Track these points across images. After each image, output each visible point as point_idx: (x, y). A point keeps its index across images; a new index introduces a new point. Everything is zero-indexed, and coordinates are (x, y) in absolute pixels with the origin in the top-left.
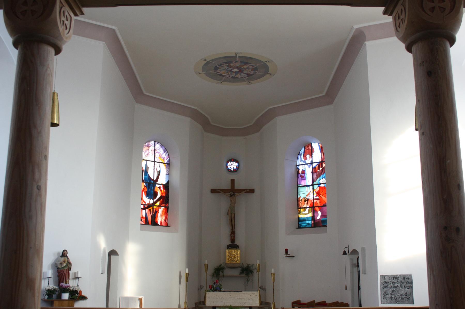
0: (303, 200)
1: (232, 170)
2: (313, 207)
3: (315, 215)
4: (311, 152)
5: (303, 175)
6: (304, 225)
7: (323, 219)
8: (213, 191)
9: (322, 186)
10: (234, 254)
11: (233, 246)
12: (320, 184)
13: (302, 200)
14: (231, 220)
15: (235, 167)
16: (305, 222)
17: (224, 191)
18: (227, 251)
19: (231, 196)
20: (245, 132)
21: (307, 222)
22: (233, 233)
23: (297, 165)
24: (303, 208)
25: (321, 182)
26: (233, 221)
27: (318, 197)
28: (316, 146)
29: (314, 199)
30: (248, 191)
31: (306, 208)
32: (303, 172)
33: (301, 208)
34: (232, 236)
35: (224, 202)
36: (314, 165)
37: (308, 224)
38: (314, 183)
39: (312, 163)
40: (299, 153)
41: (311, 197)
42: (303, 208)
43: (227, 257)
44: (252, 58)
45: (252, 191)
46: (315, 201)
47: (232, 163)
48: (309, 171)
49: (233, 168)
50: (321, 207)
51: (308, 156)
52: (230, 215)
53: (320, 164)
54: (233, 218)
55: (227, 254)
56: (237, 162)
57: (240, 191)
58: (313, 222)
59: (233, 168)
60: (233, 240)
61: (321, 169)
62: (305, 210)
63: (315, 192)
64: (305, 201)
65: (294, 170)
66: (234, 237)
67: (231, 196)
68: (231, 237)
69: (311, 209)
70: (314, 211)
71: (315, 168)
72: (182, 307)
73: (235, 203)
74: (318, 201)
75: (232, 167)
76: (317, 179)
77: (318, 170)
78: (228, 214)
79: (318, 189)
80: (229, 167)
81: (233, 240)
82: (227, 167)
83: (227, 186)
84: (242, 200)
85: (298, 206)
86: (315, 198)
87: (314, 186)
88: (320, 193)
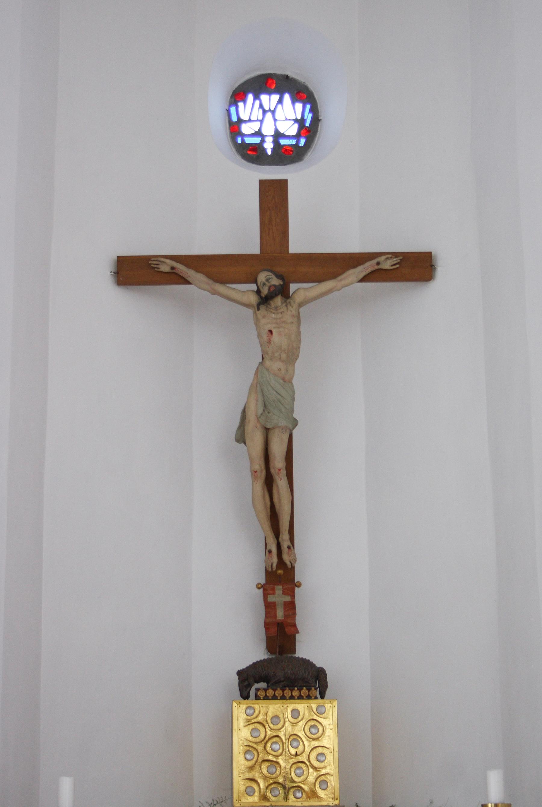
1: (269, 146)
8: (133, 272)
10: (294, 738)
11: (283, 671)
14: (269, 482)
15: (293, 130)
17: (218, 269)
18: (240, 711)
19: (264, 301)
20: (303, 753)
22: (280, 577)
26: (281, 482)
30: (387, 265)
34: (279, 597)
35: (209, 354)
43: (240, 762)
44: (260, 344)
45: (417, 267)
47: (269, 100)
49: (278, 135)
52: (256, 440)
54: (278, 463)
55: (242, 734)
56: (301, 93)
57: (331, 266)
59: (278, 135)
60: (281, 633)
66: (291, 607)
67: (264, 301)
68: (270, 607)
73: (292, 355)
75: (268, 130)
78: (241, 438)
80: (246, 129)
81: (281, 633)
82: (234, 128)
83: (236, 231)
84: (347, 352)
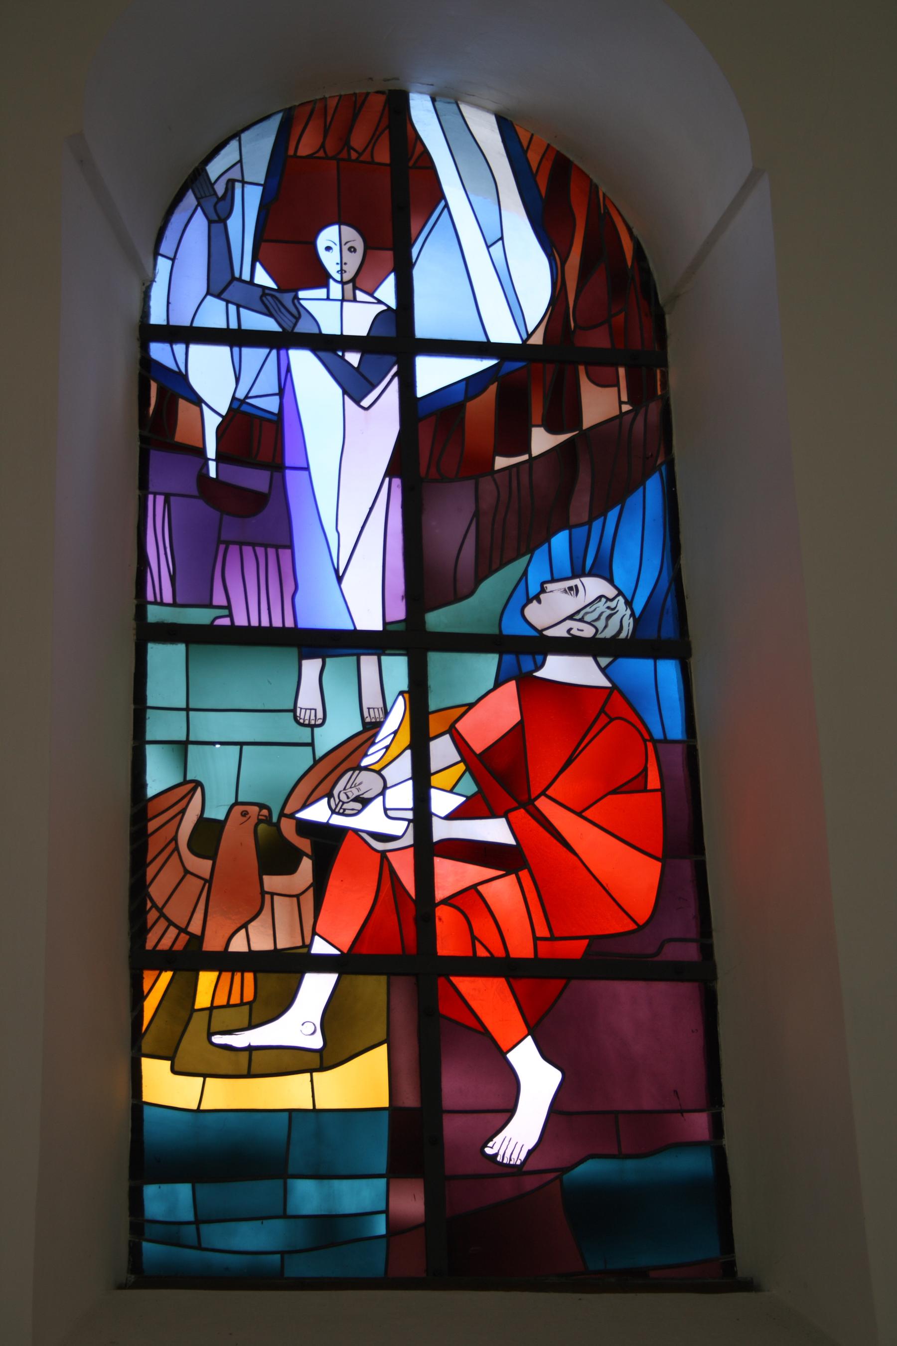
0: (239, 842)
2: (412, 973)
3: (457, 1085)
4: (396, 207)
5: (255, 480)
6: (252, 1238)
7: (590, 1169)
9: (558, 668)
12: (545, 645)
13: (208, 835)
16: (260, 1191)
21: (308, 1195)
23: (150, 334)
24: (226, 962)
25: (554, 609)
27: (495, 831)
28: (464, 151)
29: (426, 849)
31: (291, 965)
32: (262, 437)
33: (190, 959)
36: (434, 374)
37: (330, 1229)
38: (438, 620)
39: (396, 342)
40: (196, 179)
41: (382, 816)
42: (226, 962)
46: (451, 876)
48: (344, 452)
50: (554, 993)
51: (332, 245)
53: (525, 378)
58: (411, 1203)
61: (542, 441)
62: (279, 1004)
63: (442, 751)
64: (277, 856)
65: (99, 403)
69: (373, 987)
70: (442, 1056)
71: (451, 403)
72: (623, 635)
74: (503, 892)
76: (485, 569)
77: (486, 470)
79: (501, 712)
85: (139, 929)
86: (441, 831)
87: (438, 662)
88: (540, 769)
